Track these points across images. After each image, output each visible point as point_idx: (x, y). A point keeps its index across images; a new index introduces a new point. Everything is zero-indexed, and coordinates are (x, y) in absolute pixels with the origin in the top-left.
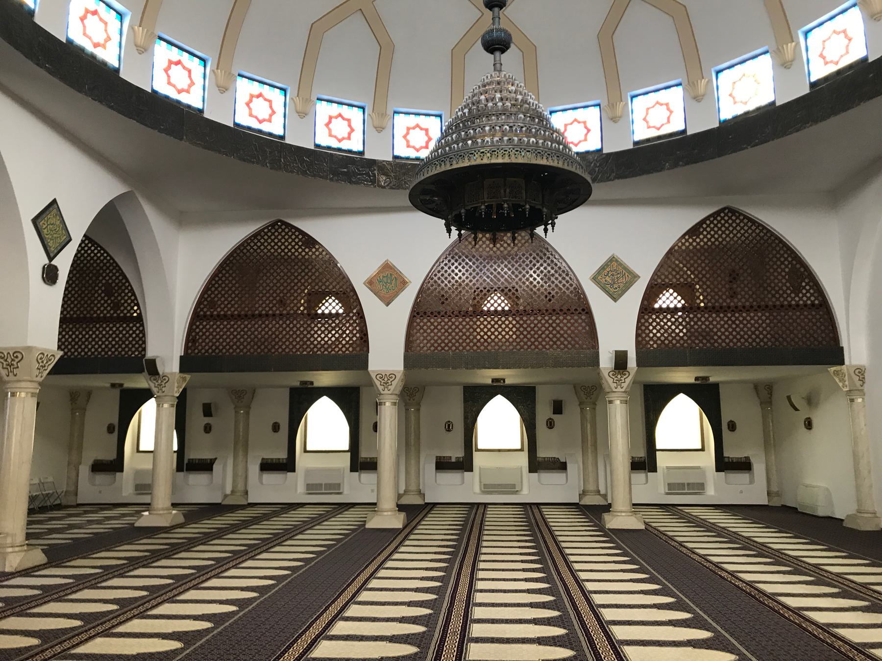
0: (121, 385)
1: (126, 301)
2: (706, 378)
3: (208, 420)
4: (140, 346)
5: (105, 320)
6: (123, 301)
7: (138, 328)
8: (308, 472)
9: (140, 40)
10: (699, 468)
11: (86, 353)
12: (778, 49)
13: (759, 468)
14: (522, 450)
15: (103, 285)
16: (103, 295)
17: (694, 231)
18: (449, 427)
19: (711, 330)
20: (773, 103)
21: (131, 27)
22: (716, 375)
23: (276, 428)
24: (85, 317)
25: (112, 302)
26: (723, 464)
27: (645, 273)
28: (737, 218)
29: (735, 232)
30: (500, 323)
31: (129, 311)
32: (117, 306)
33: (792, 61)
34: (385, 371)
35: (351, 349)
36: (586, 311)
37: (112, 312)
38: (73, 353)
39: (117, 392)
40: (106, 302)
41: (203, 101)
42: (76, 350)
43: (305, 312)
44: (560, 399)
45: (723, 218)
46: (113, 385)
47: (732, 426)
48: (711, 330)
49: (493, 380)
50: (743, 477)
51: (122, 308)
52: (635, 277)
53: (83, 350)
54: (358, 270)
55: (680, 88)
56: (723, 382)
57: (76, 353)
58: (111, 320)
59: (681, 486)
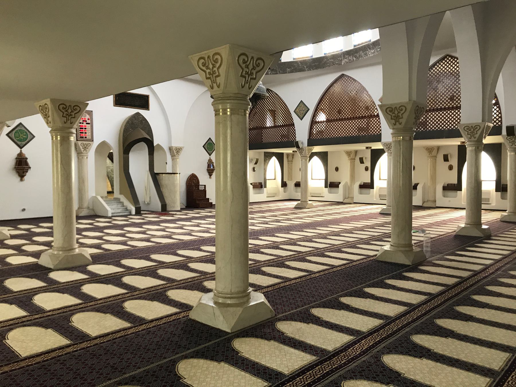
0: (371, 148)
4: (379, 129)
7: (377, 120)
11: (439, 128)
18: (451, 168)
19: (358, 127)
24: (287, 125)
27: (312, 107)
28: (454, 60)
31: (373, 113)
32: (339, 112)
39: (369, 150)
46: (367, 148)
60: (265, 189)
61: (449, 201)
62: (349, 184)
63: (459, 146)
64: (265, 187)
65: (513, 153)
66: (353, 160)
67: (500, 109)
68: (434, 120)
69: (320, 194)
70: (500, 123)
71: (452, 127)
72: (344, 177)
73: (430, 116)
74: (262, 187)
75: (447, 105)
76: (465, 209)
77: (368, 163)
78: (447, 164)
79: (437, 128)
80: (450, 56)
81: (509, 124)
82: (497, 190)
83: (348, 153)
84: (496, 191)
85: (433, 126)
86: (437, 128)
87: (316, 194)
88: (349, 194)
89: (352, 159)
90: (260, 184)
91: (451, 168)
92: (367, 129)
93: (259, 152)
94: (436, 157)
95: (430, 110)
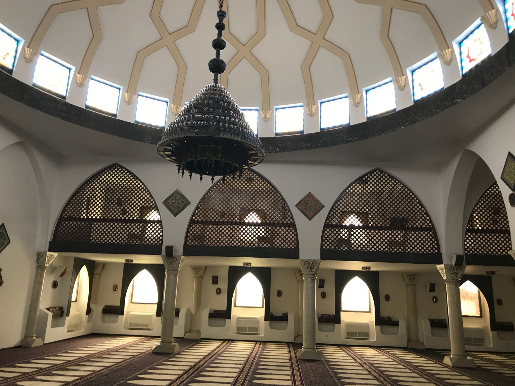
1: (130, 210)
2: (369, 268)
3: (322, 290)
5: (116, 221)
6: (128, 210)
8: (348, 325)
9: (27, 55)
10: (256, 318)
12: (396, 79)
13: (402, 325)
14: (262, 307)
15: (117, 199)
16: (116, 205)
17: (361, 180)
20: (395, 110)
21: (23, 48)
22: (374, 267)
23: (115, 288)
25: (122, 210)
26: (269, 316)
29: (391, 183)
30: (225, 229)
32: (124, 212)
33: (404, 86)
34: (310, 260)
35: (126, 241)
36: (293, 225)
37: (283, 220)
38: (108, 241)
40: (118, 210)
41: (67, 92)
42: (110, 239)
43: (238, 221)
44: (323, 279)
45: (375, 175)
47: (387, 298)
48: (388, 241)
49: (244, 264)
50: (282, 324)
51: (127, 214)
52: (188, 203)
53: (226, 242)
54: (292, 198)
55: (347, 98)
56: (275, 268)
57: (118, 241)
58: (121, 221)
59: (354, 334)
60: (67, 318)
61: (327, 336)
62: (193, 311)
63: (125, 264)
64: (68, 315)
65: (452, 286)
66: (200, 279)
67: (162, 228)
68: (214, 235)
69: (147, 325)
70: (295, 246)
71: (282, 245)
72: (186, 302)
73: (244, 229)
74: (62, 315)
75: (115, 216)
76: (159, 337)
77: (223, 285)
78: (216, 287)
79: (102, 241)
80: (119, 165)
81: (169, 244)
82: (266, 319)
83: (196, 269)
84: (266, 320)
85: (118, 239)
86: (231, 244)
87: (140, 325)
88: (191, 326)
89: (199, 277)
90: (61, 309)
91: (219, 291)
92: (403, 243)
93: (66, 258)
94: (202, 277)
95: (413, 229)
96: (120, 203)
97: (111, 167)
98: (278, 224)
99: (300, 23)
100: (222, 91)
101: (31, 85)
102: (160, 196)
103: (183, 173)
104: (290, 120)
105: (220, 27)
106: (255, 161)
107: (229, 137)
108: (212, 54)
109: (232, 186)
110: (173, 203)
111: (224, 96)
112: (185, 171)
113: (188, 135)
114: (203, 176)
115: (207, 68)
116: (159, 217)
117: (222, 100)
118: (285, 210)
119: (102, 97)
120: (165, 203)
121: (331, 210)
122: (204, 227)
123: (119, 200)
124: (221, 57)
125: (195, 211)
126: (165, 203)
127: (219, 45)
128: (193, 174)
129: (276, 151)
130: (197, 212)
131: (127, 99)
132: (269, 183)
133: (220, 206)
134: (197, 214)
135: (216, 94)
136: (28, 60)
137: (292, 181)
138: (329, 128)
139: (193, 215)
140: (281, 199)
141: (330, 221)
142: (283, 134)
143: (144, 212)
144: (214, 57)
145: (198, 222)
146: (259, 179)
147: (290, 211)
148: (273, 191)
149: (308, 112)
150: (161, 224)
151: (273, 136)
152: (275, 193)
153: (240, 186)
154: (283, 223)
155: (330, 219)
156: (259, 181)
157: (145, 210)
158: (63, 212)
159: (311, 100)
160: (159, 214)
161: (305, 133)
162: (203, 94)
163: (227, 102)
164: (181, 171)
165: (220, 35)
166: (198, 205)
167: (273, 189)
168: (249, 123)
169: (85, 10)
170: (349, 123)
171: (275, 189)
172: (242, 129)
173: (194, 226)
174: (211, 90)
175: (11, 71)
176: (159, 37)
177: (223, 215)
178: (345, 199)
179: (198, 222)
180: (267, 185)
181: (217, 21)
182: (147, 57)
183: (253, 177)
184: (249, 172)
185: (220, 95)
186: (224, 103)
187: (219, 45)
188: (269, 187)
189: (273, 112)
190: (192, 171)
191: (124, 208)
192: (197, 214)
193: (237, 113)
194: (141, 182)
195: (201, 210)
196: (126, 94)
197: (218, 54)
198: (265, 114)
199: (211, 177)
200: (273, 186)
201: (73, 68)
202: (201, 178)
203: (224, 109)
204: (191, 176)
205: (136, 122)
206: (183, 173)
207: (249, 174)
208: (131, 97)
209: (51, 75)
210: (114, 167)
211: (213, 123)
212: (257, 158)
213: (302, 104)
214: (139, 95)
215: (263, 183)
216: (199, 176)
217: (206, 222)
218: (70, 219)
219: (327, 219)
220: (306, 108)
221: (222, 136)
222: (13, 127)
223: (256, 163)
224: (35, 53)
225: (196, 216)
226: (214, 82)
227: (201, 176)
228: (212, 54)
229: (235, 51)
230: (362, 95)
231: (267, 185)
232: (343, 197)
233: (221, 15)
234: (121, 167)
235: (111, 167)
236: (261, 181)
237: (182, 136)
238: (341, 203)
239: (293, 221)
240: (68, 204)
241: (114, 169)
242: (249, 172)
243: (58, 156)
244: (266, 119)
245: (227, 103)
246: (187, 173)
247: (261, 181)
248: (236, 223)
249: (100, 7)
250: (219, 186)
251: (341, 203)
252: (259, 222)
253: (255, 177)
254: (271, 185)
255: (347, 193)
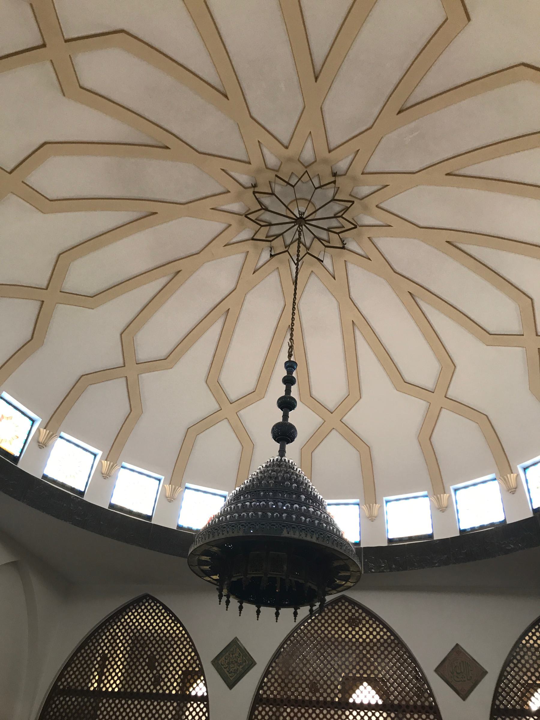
9: (42, 439)
32: (157, 680)
41: (86, 486)
54: (429, 657)
55: (496, 482)
67: (208, 711)
96: (152, 667)
97: (137, 602)
98: (408, 706)
99: (407, 379)
100: (290, 467)
101: (40, 477)
102: (209, 649)
103: (228, 602)
104: (408, 518)
105: (289, 381)
106: (346, 579)
107: (297, 536)
108: (277, 416)
109: (323, 632)
110: (229, 664)
111: (293, 473)
112: (231, 599)
113: (233, 535)
114: (262, 609)
115: (270, 436)
116: (204, 689)
117: (290, 479)
118: (417, 679)
119: (135, 492)
120: (215, 662)
121: (500, 681)
122: (278, 710)
123: (152, 658)
124: (290, 421)
125: (263, 679)
126: (215, 662)
127: (287, 404)
128: (244, 605)
129: (391, 570)
130: (266, 680)
131: (168, 493)
132: (385, 626)
133: (304, 670)
134: (266, 684)
135: (281, 471)
136: (41, 445)
137: (425, 625)
138: (473, 529)
139: (260, 687)
140: (409, 657)
141: (501, 702)
142: (401, 540)
143: (189, 681)
144: (280, 420)
145: (268, 702)
146: (367, 618)
147: (427, 682)
148: (393, 641)
149: (437, 506)
150: (208, 704)
151: (385, 544)
152: (396, 645)
153: (336, 632)
154: (415, 706)
155: (500, 698)
156: (367, 622)
157: (190, 677)
158: (59, 679)
159: (438, 485)
160: (205, 685)
161: (435, 539)
162: (261, 472)
163: (296, 482)
164: (224, 599)
165: (288, 391)
166: (269, 668)
167: (392, 638)
168: (331, 515)
169: (124, 379)
170: (505, 521)
171: (397, 637)
172: (335, 536)
173: (260, 709)
174: (274, 465)
175: (16, 459)
176: (217, 407)
177: (314, 687)
178: (522, 657)
179: (268, 702)
180: (381, 630)
181: (285, 373)
182: (200, 435)
183: (357, 614)
184: (350, 607)
185: (288, 473)
186: (292, 484)
187: (287, 404)
188: (385, 633)
189: (381, 507)
190: (243, 598)
191: (158, 672)
192: (266, 684)
193: (318, 503)
194: (182, 625)
195: (273, 677)
196: (167, 486)
197: (286, 417)
198: (370, 509)
199: (274, 610)
200: (393, 633)
201: (100, 453)
202: (258, 612)
203: (291, 492)
204: (241, 608)
205: (179, 527)
206: (228, 602)
207: (350, 611)
208: (174, 491)
209: (68, 465)
210: (144, 601)
211: (273, 514)
212: (348, 574)
213: (425, 493)
214: (186, 488)
215: (374, 626)
216: (254, 608)
217: (282, 700)
218: (69, 692)
219: (495, 697)
220: (433, 499)
221: (285, 534)
222: (12, 542)
223: (349, 584)
224: (53, 434)
225: (265, 688)
226: (279, 455)
227: (259, 607)
228: (277, 416)
229: (320, 420)
230: (518, 475)
231: (381, 630)
232: (518, 653)
233: (290, 366)
234: (154, 600)
235: (137, 602)
236: (371, 622)
237: (223, 537)
238: (516, 665)
239: (434, 700)
240: (68, 665)
241: (144, 604)
242: (350, 607)
243: (64, 583)
244: (372, 518)
245: (296, 483)
246: (234, 602)
247: (371, 622)
248: (333, 705)
249: (143, 375)
250: (302, 631)
251: (516, 665)
252: (380, 702)
253: (360, 615)
254: (389, 629)
255: (524, 645)
